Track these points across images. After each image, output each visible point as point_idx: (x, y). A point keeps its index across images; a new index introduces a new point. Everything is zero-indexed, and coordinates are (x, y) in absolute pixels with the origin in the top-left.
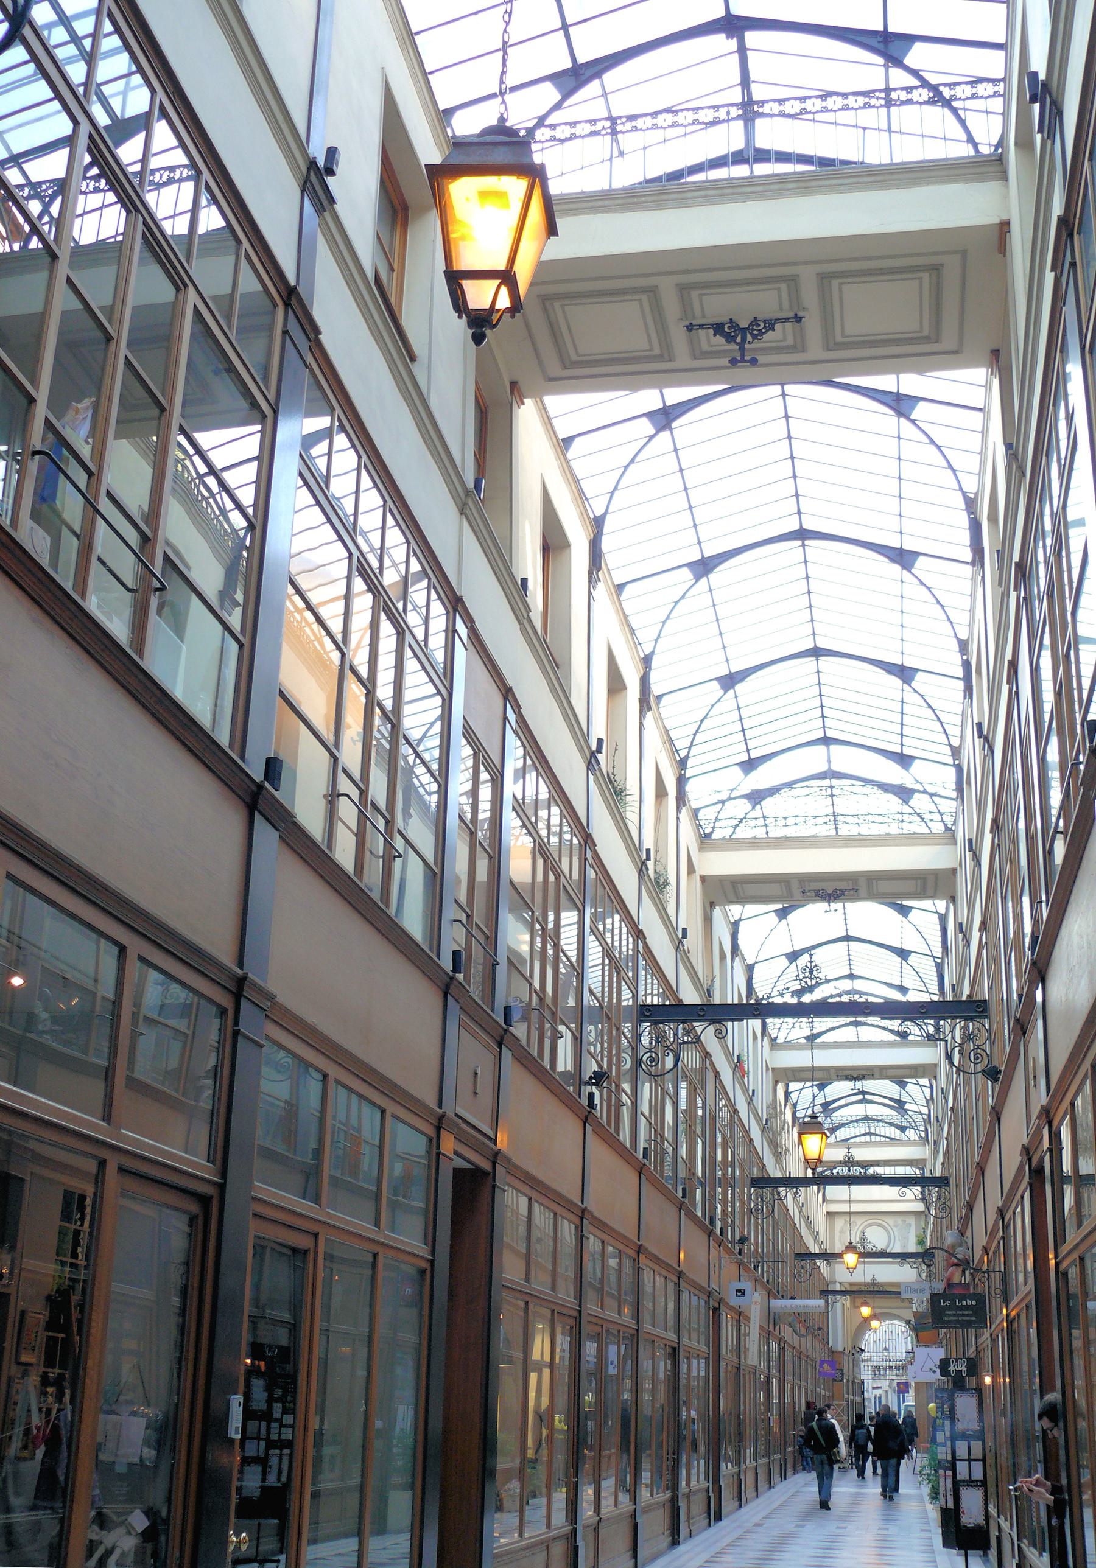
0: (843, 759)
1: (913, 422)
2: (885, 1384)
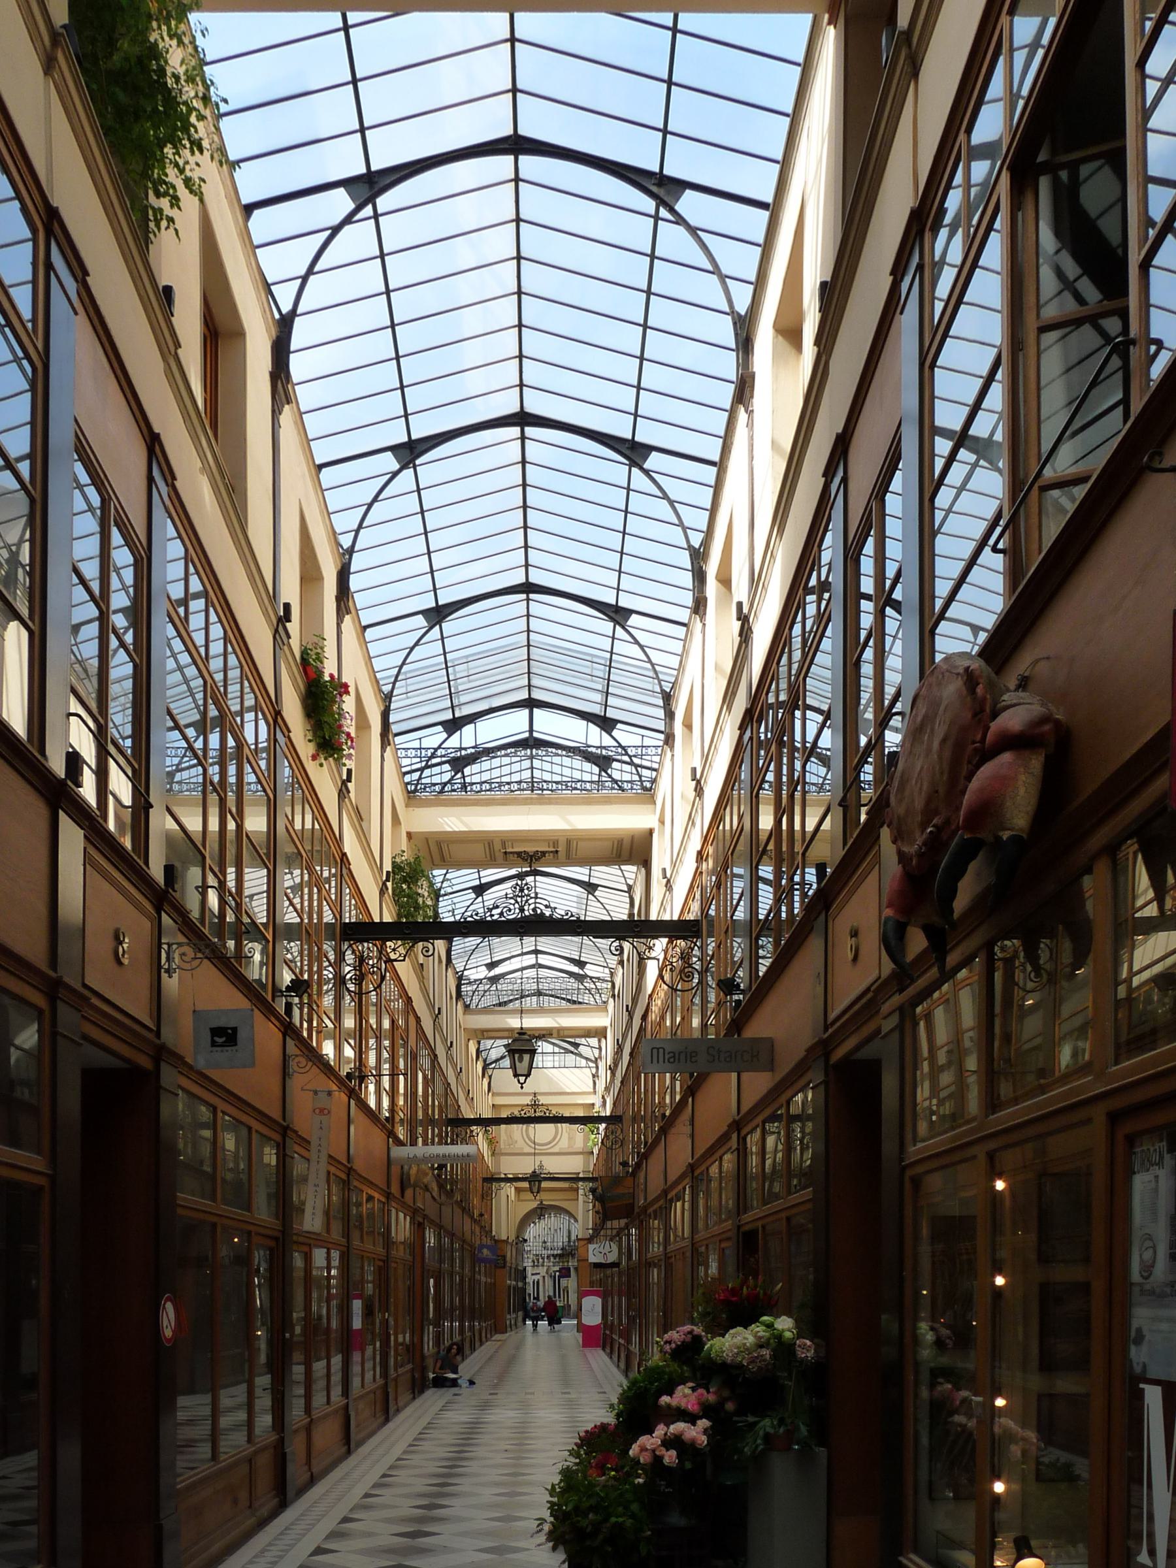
0: (548, 724)
1: (647, 472)
2: (542, 1271)
